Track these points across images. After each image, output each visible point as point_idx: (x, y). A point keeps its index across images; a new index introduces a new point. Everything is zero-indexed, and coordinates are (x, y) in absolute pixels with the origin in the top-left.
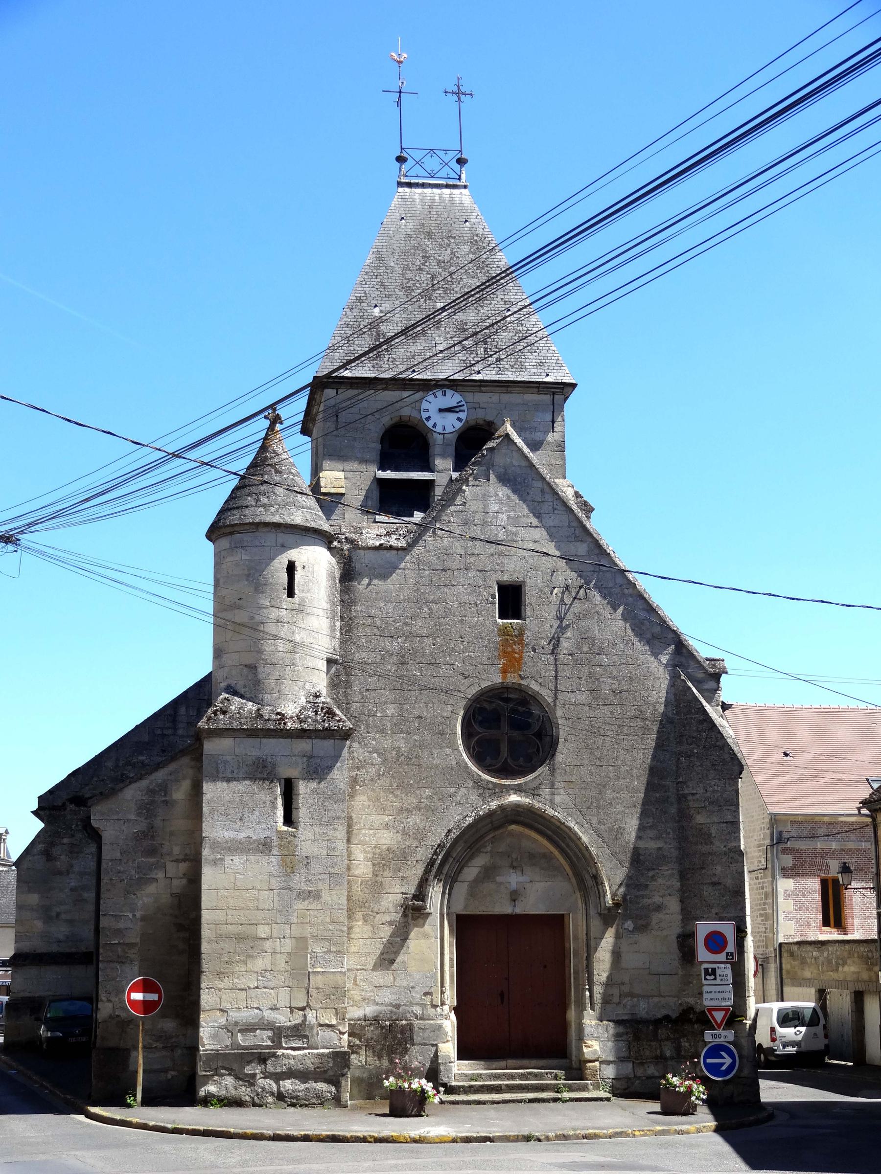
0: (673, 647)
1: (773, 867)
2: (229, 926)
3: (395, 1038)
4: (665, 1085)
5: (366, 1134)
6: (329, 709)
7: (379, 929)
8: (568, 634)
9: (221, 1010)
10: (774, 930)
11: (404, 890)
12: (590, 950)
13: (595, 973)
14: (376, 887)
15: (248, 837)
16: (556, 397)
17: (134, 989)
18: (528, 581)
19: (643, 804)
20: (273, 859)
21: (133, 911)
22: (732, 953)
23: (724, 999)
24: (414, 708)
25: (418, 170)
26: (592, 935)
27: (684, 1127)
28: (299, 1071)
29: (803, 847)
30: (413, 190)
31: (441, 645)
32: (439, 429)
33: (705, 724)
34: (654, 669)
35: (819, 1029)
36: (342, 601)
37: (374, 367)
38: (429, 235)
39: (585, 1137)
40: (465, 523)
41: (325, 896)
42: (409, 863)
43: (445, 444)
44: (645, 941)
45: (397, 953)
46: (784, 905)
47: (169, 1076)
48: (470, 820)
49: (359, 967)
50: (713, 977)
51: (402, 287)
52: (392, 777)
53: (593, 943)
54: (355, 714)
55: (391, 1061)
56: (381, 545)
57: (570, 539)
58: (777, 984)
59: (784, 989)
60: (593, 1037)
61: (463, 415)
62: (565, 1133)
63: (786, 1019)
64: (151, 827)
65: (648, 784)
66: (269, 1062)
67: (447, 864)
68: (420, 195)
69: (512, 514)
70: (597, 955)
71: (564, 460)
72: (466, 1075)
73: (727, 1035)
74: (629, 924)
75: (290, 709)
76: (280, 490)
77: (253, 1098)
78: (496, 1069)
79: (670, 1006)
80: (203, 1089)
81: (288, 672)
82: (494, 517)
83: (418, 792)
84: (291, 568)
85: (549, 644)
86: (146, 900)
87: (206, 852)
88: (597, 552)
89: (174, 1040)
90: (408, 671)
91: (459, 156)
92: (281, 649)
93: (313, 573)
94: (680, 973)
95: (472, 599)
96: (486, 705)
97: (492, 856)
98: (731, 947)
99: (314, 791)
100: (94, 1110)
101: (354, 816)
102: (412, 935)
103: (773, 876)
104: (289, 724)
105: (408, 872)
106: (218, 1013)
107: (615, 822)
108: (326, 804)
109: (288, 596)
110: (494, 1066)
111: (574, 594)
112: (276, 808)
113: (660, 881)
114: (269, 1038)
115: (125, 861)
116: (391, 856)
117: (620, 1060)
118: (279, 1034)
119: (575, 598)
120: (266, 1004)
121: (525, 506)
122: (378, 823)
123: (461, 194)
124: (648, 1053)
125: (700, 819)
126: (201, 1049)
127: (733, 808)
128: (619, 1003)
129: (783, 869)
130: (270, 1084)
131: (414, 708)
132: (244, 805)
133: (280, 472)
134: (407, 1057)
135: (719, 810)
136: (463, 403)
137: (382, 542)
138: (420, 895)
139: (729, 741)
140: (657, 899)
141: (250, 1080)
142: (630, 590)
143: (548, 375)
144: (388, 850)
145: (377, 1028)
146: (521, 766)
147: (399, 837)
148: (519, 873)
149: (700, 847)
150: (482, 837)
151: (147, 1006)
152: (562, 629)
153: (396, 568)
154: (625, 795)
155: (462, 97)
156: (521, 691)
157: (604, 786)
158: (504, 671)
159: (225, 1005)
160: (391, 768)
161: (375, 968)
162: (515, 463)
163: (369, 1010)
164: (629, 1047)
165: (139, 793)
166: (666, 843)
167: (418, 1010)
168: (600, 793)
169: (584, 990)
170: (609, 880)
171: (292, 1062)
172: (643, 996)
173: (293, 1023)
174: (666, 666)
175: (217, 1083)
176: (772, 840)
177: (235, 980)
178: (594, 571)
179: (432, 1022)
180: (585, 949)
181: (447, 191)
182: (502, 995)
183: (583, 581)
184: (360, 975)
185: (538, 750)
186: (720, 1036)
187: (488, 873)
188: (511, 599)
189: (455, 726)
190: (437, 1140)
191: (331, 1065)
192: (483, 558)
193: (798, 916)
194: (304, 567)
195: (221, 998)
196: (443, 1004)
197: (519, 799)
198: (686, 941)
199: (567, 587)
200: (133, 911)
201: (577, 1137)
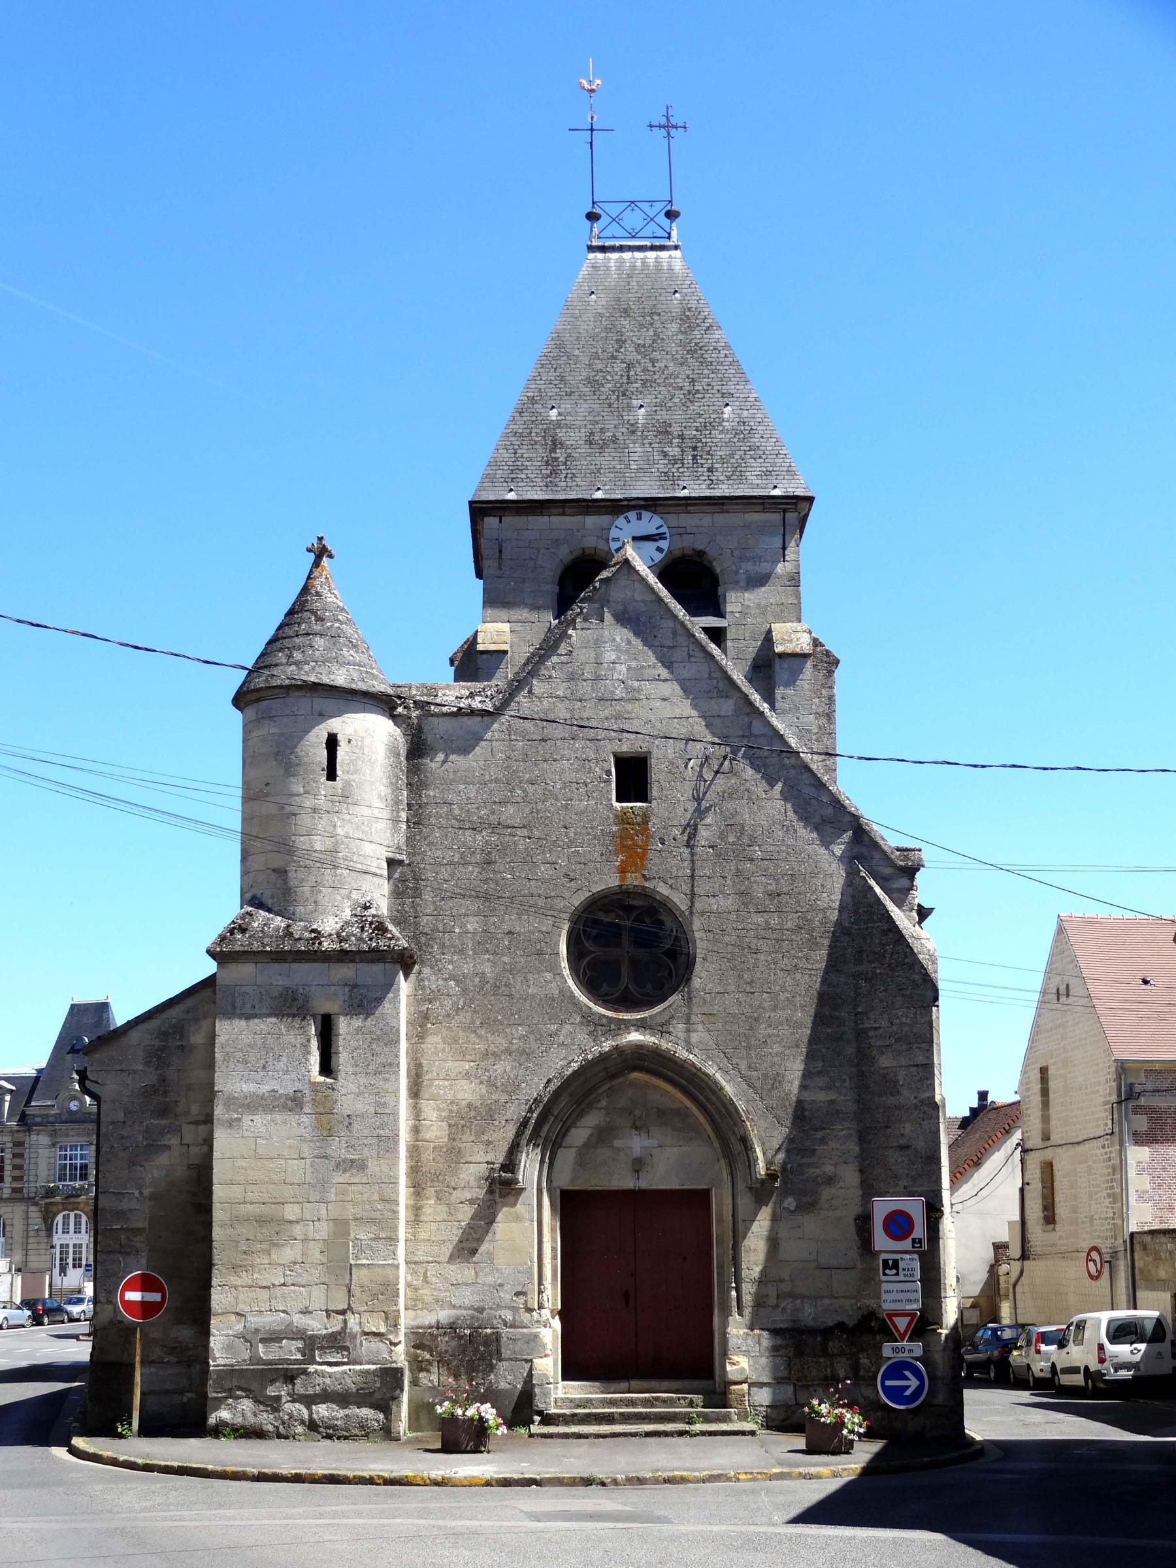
0: (850, 833)
1: (1121, 1131)
2: (248, 1206)
3: (476, 1350)
4: (810, 1414)
5: (373, 1474)
6: (381, 923)
7: (456, 1210)
8: (708, 820)
9: (237, 1314)
10: (1123, 1216)
11: (489, 1158)
13: (744, 1266)
14: (453, 1154)
15: (274, 1091)
17: (129, 1287)
18: (655, 751)
19: (810, 1043)
20: (305, 1119)
22: (920, 1240)
23: (909, 1301)
24: (503, 921)
25: (615, 229)
26: (740, 1217)
27: (813, 1470)
29: (1163, 1105)
30: (608, 255)
33: (891, 935)
35: (1165, 1347)
36: (409, 784)
37: (547, 486)
38: (626, 312)
39: (667, 1481)
40: (571, 678)
41: (372, 1165)
42: (497, 1123)
44: (811, 1224)
45: (480, 1240)
46: (1137, 1181)
47: (185, 1400)
49: (430, 1259)
50: (894, 1271)
51: (589, 381)
52: (475, 1012)
53: (741, 1228)
54: (426, 930)
57: (710, 695)
58: (1127, 1287)
59: (1138, 1294)
60: (739, 1351)
61: (664, 544)
62: (640, 1475)
63: (1121, 1332)
65: (817, 1015)
66: (298, 1381)
67: (549, 1123)
68: (617, 261)
69: (634, 664)
70: (746, 1243)
71: (798, 597)
72: (571, 1400)
74: (790, 1203)
75: (329, 925)
76: (319, 642)
77: (277, 1427)
78: (614, 1393)
79: (846, 1311)
80: (213, 1415)
81: (327, 877)
82: (609, 669)
83: (508, 1030)
84: (332, 743)
85: (683, 832)
86: (156, 1173)
87: (219, 1111)
88: (748, 710)
89: (191, 1353)
91: (668, 208)
92: (318, 847)
93: (362, 748)
94: (859, 1266)
95: (582, 777)
96: (602, 917)
97: (607, 1114)
98: (919, 1231)
99: (358, 1030)
100: (79, 1442)
101: (424, 1062)
103: (1121, 1144)
104: (325, 944)
105: (495, 1135)
106: (233, 1318)
107: (771, 1067)
108: (374, 1046)
110: (612, 1389)
111: (716, 768)
112: (309, 1053)
113: (832, 1144)
114: (299, 1349)
115: (129, 1123)
116: (473, 1114)
117: (779, 1381)
118: (312, 1345)
119: (717, 772)
120: (295, 1306)
121: (650, 653)
122: (455, 1071)
123: (670, 257)
124: (814, 1373)
125: (885, 1061)
128: (777, 1306)
129: (1135, 1133)
131: (503, 921)
132: (268, 1049)
133: (322, 620)
134: (492, 1376)
135: (908, 1050)
136: (664, 529)
138: (510, 1165)
139: (921, 957)
140: (828, 1169)
141: (274, 1405)
143: (775, 487)
144: (470, 1106)
145: (453, 1338)
146: (648, 995)
149: (884, 1098)
150: (594, 1089)
151: (146, 1309)
152: (700, 813)
154: (785, 1031)
155: (673, 132)
157: (757, 1020)
158: (623, 871)
159: (242, 1308)
160: (472, 1000)
161: (451, 1260)
162: (638, 597)
163: (444, 1315)
164: (789, 1365)
165: (148, 1036)
166: (840, 1093)
167: (508, 1316)
169: (730, 1288)
170: (763, 1144)
171: (328, 1381)
172: (809, 1298)
173: (330, 1330)
174: (841, 859)
175: (231, 1408)
176: (1119, 1095)
177: (256, 1276)
178: (743, 736)
179: (525, 1330)
180: (731, 1234)
181: (651, 255)
182: (626, 1296)
184: (432, 1270)
185: (670, 974)
186: (903, 1350)
187: (603, 1136)
188: (633, 776)
189: (557, 943)
190: (466, 1483)
191: (378, 1385)
193: (1156, 1197)
194: (349, 741)
195: (237, 1298)
196: (541, 1307)
197: (641, 1038)
198: (864, 1221)
199: (707, 758)
200: (140, 1188)
201: (656, 1481)
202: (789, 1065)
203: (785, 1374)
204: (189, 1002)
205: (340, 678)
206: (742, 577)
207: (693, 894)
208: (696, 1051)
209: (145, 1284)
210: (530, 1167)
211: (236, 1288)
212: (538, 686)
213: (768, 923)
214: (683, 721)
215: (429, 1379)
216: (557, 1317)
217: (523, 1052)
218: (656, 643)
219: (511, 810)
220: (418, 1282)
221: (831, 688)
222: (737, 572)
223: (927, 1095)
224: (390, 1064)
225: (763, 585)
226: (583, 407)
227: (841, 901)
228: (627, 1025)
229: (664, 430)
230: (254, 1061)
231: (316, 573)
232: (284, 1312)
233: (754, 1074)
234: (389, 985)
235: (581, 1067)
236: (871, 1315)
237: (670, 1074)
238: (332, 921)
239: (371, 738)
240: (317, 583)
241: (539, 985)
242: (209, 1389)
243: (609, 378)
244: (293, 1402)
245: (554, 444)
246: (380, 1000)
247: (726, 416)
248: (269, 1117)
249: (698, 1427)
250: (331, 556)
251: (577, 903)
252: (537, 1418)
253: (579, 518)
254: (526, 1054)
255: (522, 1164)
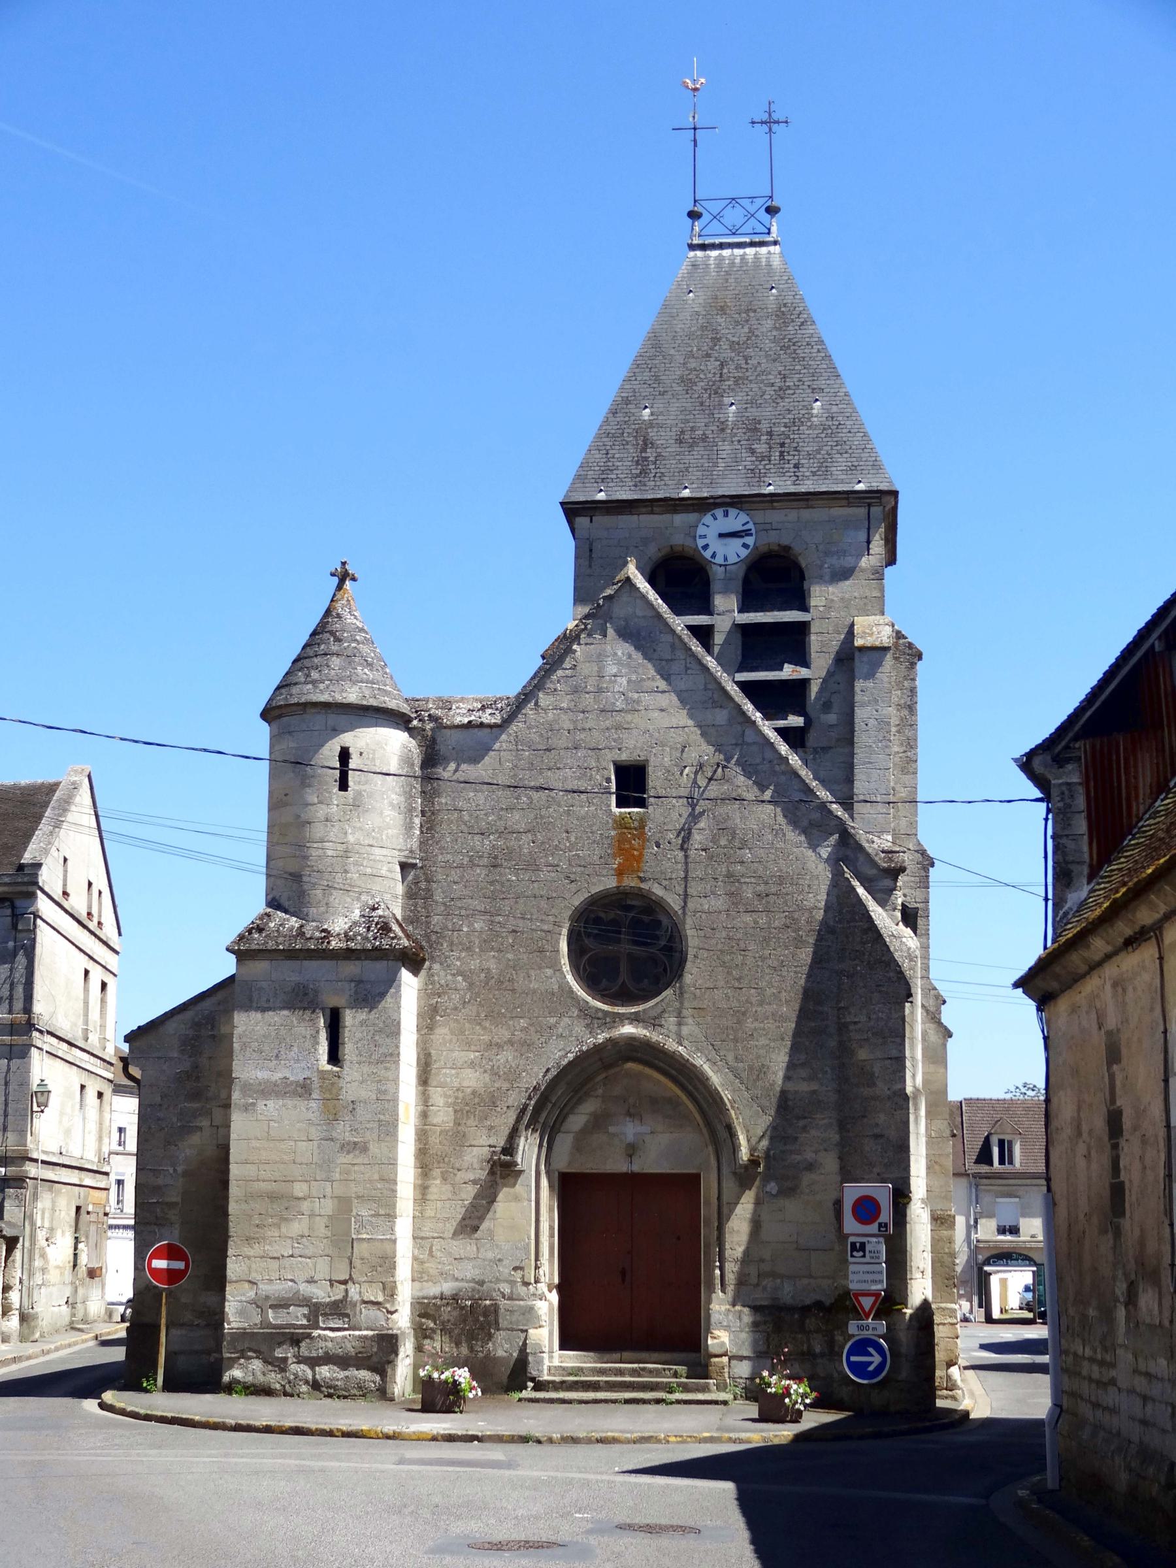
0: (836, 836)
2: (261, 1183)
4: (760, 1384)
5: (332, 1427)
6: (386, 924)
8: (702, 825)
9: (250, 1282)
11: (492, 1141)
12: (722, 1219)
13: (727, 1246)
14: (458, 1138)
15: (285, 1078)
16: (872, 509)
20: (313, 1104)
21: (174, 1165)
22: (886, 1225)
23: (874, 1282)
25: (715, 227)
26: (725, 1199)
28: (341, 1357)
30: (708, 252)
31: (543, 843)
32: (719, 560)
34: (811, 865)
36: (423, 792)
37: (636, 486)
38: (723, 310)
39: (600, 1441)
40: (575, 691)
41: (374, 1148)
43: (728, 579)
44: (792, 1208)
45: (482, 1218)
48: (571, 1056)
50: (861, 1254)
53: (725, 1210)
54: (437, 929)
55: (471, 1349)
56: (470, 722)
61: (750, 541)
62: (575, 1435)
64: (196, 1067)
66: (303, 1344)
67: (548, 1110)
69: (634, 677)
70: (730, 1224)
71: (882, 590)
72: (564, 1369)
73: (876, 1328)
74: (772, 1187)
76: (335, 662)
82: (611, 682)
84: (345, 755)
85: (678, 836)
87: (236, 1096)
88: (741, 719)
90: (501, 874)
91: (769, 204)
93: (373, 759)
98: (886, 1215)
99: (363, 1023)
101: (433, 1052)
102: (500, 1197)
104: (333, 943)
106: (246, 1285)
108: (377, 1038)
109: (340, 789)
111: (710, 775)
112: (318, 1043)
113: (813, 1132)
114: (304, 1315)
116: (477, 1100)
118: (316, 1311)
119: (710, 779)
120: (301, 1276)
121: (650, 666)
123: (769, 253)
125: (863, 1054)
126: (226, 1326)
127: (898, 1040)
128: (758, 1285)
130: (304, 1370)
134: (490, 1344)
136: (750, 526)
137: (473, 718)
138: (509, 1149)
139: (896, 955)
140: (809, 1155)
141: (281, 1365)
142: (783, 767)
144: (474, 1093)
145: (455, 1308)
147: (487, 1077)
148: (637, 1122)
150: (590, 1079)
151: (172, 1276)
152: (694, 817)
153: (489, 749)
154: (770, 1025)
156: (643, 896)
157: (744, 1014)
158: (620, 873)
159: (254, 1276)
160: (478, 994)
162: (639, 613)
163: (447, 1287)
165: (183, 1026)
166: (822, 1084)
168: (739, 1022)
171: (330, 1344)
173: (333, 1299)
174: (827, 861)
175: (242, 1366)
178: (736, 745)
180: (716, 1216)
181: (750, 251)
183: (722, 757)
185: (665, 970)
186: (867, 1327)
187: (598, 1122)
188: (632, 782)
191: (375, 1350)
192: (595, 733)
194: (361, 754)
195: (250, 1268)
198: (838, 1204)
199: (701, 766)
200: (174, 1165)
201: (589, 1441)
202: (774, 1056)
203: (763, 1348)
204: (220, 996)
205: (352, 695)
206: (827, 571)
207: (686, 895)
208: (686, 1043)
209: (171, 1253)
210: (528, 1151)
211: (249, 1258)
212: (544, 699)
213: (756, 922)
214: (680, 731)
215: (436, 1344)
216: (555, 1291)
217: (524, 1043)
218: (655, 656)
219: (517, 816)
220: (424, 1256)
221: (914, 680)
222: (821, 567)
223: (899, 1086)
224: (391, 1055)
225: (847, 578)
226: (675, 406)
227: (827, 901)
228: (622, 1019)
229: (753, 428)
230: (269, 1049)
231: (338, 596)
232: (292, 1280)
233: (741, 1065)
234: (392, 980)
235: (576, 1058)
236: (846, 1294)
237: (661, 1064)
238: (341, 920)
239: (386, 748)
240: (338, 605)
241: (539, 981)
242: (224, 1350)
243: (702, 376)
244: (299, 1362)
245: (645, 444)
246: (383, 995)
247: (815, 411)
248: (281, 1102)
249: (678, 1396)
250: (354, 579)
251: (577, 903)
252: (531, 1384)
253: (667, 517)
254: (527, 1045)
255: (521, 1148)
